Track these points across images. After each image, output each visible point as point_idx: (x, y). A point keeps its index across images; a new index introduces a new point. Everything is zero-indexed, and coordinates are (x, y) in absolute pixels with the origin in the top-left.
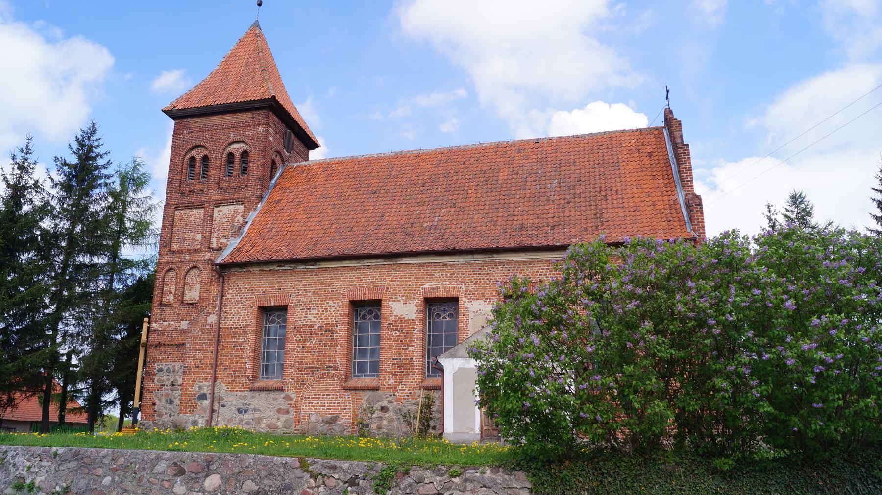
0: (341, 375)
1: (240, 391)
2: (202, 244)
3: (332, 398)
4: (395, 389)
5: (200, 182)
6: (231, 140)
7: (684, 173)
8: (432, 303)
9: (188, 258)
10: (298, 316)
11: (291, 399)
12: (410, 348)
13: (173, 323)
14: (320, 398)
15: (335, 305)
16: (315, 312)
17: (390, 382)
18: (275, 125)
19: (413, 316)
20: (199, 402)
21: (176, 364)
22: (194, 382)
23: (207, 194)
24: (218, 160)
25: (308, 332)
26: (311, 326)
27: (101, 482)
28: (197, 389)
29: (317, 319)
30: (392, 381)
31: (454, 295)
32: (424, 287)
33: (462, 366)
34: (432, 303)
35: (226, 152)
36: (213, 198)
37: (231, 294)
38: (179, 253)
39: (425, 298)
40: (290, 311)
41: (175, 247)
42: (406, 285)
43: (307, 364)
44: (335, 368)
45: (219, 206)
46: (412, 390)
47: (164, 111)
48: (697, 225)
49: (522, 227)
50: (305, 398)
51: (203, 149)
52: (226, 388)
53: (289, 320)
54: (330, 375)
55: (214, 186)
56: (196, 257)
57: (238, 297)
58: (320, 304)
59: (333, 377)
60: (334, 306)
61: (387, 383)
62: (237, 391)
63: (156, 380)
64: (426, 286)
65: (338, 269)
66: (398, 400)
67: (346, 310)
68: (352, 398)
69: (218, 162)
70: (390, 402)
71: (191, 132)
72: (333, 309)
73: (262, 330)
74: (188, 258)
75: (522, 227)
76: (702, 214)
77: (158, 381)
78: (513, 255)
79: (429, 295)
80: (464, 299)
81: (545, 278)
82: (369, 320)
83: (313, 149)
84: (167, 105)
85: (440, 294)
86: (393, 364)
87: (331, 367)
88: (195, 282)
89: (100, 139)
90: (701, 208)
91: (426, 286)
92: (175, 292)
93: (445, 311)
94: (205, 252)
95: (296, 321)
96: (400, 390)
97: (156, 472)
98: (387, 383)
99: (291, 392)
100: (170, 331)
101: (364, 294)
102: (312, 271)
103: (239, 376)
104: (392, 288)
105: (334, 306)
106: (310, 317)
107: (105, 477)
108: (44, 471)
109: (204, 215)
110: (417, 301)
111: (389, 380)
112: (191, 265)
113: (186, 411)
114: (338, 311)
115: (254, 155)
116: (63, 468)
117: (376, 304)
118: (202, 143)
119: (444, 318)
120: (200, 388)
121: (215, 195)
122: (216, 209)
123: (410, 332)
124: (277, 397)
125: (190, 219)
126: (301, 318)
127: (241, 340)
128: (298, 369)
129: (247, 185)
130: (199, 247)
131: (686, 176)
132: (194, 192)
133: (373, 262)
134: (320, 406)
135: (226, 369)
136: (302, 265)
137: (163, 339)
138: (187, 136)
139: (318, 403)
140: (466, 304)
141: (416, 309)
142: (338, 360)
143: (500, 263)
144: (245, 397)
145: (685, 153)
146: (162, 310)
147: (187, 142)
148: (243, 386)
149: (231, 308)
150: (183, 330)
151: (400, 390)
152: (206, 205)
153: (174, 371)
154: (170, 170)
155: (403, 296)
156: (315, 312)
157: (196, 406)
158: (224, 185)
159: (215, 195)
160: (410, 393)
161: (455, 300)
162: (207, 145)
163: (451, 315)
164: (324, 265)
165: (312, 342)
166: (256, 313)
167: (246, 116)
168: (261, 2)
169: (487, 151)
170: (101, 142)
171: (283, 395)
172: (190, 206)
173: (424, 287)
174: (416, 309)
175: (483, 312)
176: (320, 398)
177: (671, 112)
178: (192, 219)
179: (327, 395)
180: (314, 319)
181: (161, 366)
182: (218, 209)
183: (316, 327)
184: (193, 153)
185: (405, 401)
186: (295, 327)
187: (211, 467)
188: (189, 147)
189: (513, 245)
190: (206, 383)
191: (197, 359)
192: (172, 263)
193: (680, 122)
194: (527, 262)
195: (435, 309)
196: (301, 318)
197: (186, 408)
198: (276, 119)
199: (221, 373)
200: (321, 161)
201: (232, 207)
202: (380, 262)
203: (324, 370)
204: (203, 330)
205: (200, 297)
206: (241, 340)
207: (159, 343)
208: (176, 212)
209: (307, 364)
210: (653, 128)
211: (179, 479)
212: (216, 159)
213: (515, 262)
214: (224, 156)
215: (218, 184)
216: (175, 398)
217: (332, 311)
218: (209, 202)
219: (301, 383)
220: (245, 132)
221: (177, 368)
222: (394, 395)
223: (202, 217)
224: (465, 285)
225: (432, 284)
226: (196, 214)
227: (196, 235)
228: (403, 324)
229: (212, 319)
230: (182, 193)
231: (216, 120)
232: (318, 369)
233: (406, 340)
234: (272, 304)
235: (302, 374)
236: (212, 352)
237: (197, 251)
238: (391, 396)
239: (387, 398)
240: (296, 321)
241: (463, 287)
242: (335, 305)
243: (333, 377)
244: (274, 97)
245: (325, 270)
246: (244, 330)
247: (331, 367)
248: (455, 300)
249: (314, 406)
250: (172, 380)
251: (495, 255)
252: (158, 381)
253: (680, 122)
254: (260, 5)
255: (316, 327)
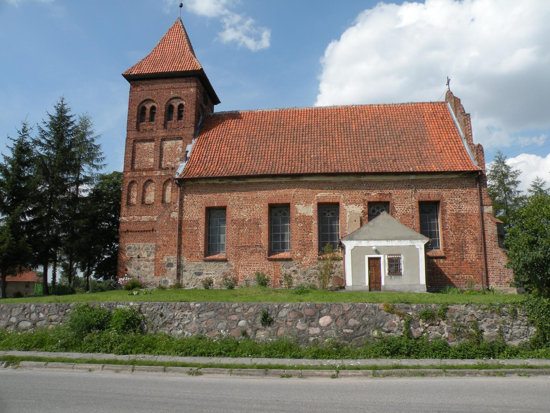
0: (265, 251)
1: (196, 261)
2: (154, 165)
3: (260, 265)
4: (301, 259)
8: (272, 207)
9: (144, 174)
10: (233, 213)
11: (232, 266)
12: (310, 234)
13: (136, 217)
14: (251, 265)
15: (259, 206)
16: (246, 210)
17: (298, 255)
19: (311, 214)
20: (168, 269)
21: (140, 244)
22: (163, 255)
23: (156, 132)
24: (161, 110)
25: (241, 223)
26: (244, 220)
27: (238, 324)
28: (166, 260)
29: (247, 215)
30: (299, 255)
31: (337, 201)
32: (317, 196)
33: (357, 245)
34: (209, 211)
36: (161, 134)
37: (187, 198)
38: (138, 171)
39: (318, 203)
40: (228, 210)
41: (136, 167)
42: (306, 195)
43: (241, 244)
44: (261, 247)
46: (313, 260)
47: (123, 75)
49: (374, 160)
50: (242, 265)
51: (179, 100)
52: (186, 259)
53: (228, 216)
54: (258, 251)
56: (150, 174)
57: (191, 200)
58: (249, 205)
59: (259, 252)
60: (258, 207)
61: (296, 255)
62: (194, 261)
63: (126, 255)
64: (319, 195)
65: (260, 183)
66: (303, 266)
67: (267, 210)
68: (274, 265)
70: (298, 268)
71: (143, 90)
72: (258, 209)
73: (208, 223)
74: (144, 174)
75: (374, 160)
76: (483, 156)
77: (128, 255)
78: (374, 177)
79: (321, 201)
80: (343, 204)
82: (279, 216)
83: (216, 104)
85: (327, 200)
86: (299, 244)
87: (258, 246)
88: (150, 190)
90: (483, 152)
91: (319, 195)
92: (137, 197)
93: (329, 211)
94: (157, 170)
95: (233, 216)
96: (305, 260)
97: (280, 316)
98: (296, 255)
99: (232, 262)
100: (135, 222)
101: (278, 200)
102: (242, 184)
103: (195, 252)
104: (297, 196)
105: (258, 207)
106: (242, 214)
107: (239, 321)
108: (187, 318)
109: (155, 146)
110: (313, 204)
111: (297, 254)
112: (147, 179)
113: (159, 274)
114: (261, 210)
116: (202, 316)
117: (287, 206)
118: (151, 98)
119: (329, 215)
120: (168, 259)
121: (162, 133)
123: (310, 224)
124: (222, 265)
125: (145, 148)
126: (236, 214)
127: (195, 228)
128: (236, 247)
129: (184, 127)
130: (152, 167)
132: (147, 130)
133: (284, 180)
134: (252, 270)
135: (185, 247)
136: (235, 180)
137: (130, 227)
138: (140, 93)
139: (250, 269)
140: (344, 207)
141: (313, 209)
142: (262, 241)
143: (365, 182)
144: (200, 265)
146: (128, 209)
147: (140, 97)
148: (198, 258)
149: (187, 208)
150: (144, 221)
151: (305, 260)
153: (139, 249)
154: (129, 115)
155: (304, 201)
156: (246, 210)
157: (166, 271)
159: (162, 133)
160: (311, 262)
161: (337, 204)
162: (155, 99)
163: (332, 214)
164: (250, 181)
165: (244, 230)
166: (204, 211)
171: (226, 264)
172: (144, 140)
173: (317, 196)
174: (313, 209)
175: (355, 212)
176: (251, 265)
177: (451, 93)
179: (256, 263)
180: (245, 215)
181: (129, 245)
183: (246, 220)
185: (308, 267)
186: (232, 221)
187: (322, 312)
188: (142, 100)
189: (374, 171)
190: (172, 257)
191: (165, 241)
192: (134, 177)
193: (460, 99)
194: (381, 181)
195: (274, 211)
196: (236, 214)
197: (158, 272)
198: (200, 84)
199: (183, 251)
200: (229, 113)
201: (174, 142)
202: (288, 179)
203: (253, 248)
204: (168, 222)
205: (155, 200)
206: (195, 228)
207: (128, 230)
209: (241, 244)
211: (299, 320)
213: (374, 181)
216: (141, 266)
217: (257, 210)
219: (238, 256)
220: (181, 91)
221: (141, 247)
222: (301, 263)
223: (153, 147)
224: (343, 195)
225: (322, 194)
226: (149, 146)
227: (149, 159)
228: (305, 219)
229: (175, 215)
232: (249, 247)
233: (307, 228)
234: (216, 205)
235: (238, 250)
236: (175, 236)
237: (152, 170)
238: (298, 263)
239: (296, 265)
240: (233, 216)
241: (342, 196)
242: (259, 206)
243: (259, 252)
244: (202, 69)
245: (251, 184)
246: (197, 222)
247: (258, 246)
248: (337, 204)
249: (247, 271)
250: (138, 254)
251: (362, 177)
252: (128, 255)
253: (460, 99)
255: (246, 220)
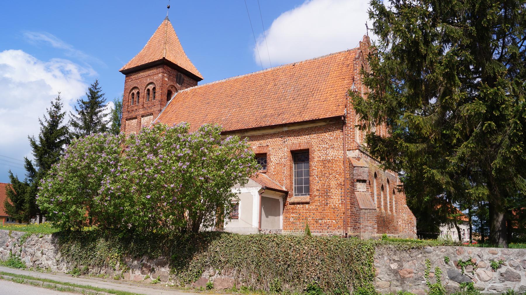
5: (136, 105)
6: (148, 83)
7: (356, 76)
10: (316, 156)
18: (169, 72)
35: (147, 89)
36: (141, 113)
45: (143, 117)
48: (349, 107)
55: (141, 107)
69: (143, 94)
79: (294, 148)
81: (269, 144)
84: (122, 69)
89: (101, 88)
115: (158, 89)
118: (136, 86)
121: (141, 112)
122: (142, 119)
131: (357, 77)
145: (356, 63)
147: (130, 86)
152: (138, 117)
158: (145, 106)
167: (154, 71)
168: (169, 6)
169: (268, 73)
170: (101, 89)
178: (133, 124)
182: (143, 118)
184: (133, 91)
188: (131, 88)
196: (335, 156)
198: (170, 69)
208: (126, 122)
210: (357, 48)
212: (142, 93)
213: (255, 136)
214: (146, 91)
215: (143, 105)
218: (139, 115)
230: (129, 112)
231: (142, 74)
254: (169, 8)
